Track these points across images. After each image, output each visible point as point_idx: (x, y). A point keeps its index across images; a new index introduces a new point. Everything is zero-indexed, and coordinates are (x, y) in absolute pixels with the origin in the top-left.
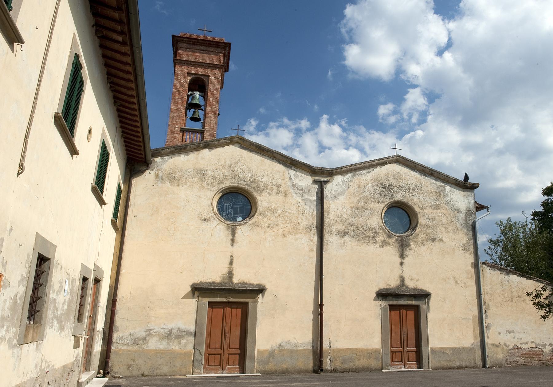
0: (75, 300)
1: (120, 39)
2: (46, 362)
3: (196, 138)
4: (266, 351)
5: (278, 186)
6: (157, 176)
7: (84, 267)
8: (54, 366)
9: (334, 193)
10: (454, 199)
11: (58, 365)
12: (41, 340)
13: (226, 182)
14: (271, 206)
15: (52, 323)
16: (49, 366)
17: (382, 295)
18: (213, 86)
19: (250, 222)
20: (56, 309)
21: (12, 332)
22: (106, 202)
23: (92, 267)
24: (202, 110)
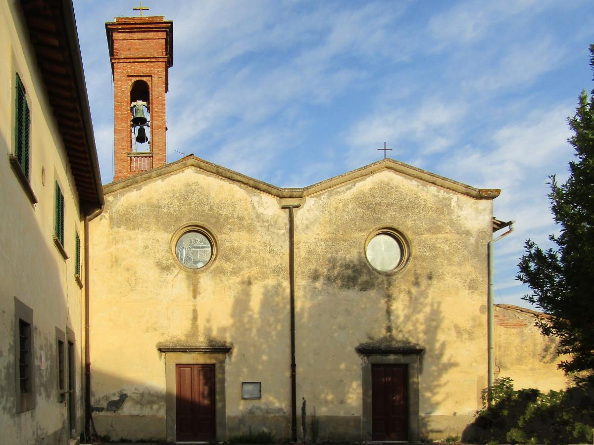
0: (493, 330)
1: (56, 42)
2: (41, 429)
3: (144, 163)
4: (236, 417)
5: (241, 219)
6: (111, 218)
7: (58, 330)
8: (47, 433)
9: (305, 222)
10: (462, 217)
11: (50, 432)
12: (34, 408)
13: (183, 219)
14: (233, 246)
15: (40, 390)
16: (43, 433)
17: (363, 351)
18: (156, 90)
19: (212, 268)
20: (41, 376)
21: (10, 401)
22: (68, 256)
23: (65, 331)
24: (148, 126)
